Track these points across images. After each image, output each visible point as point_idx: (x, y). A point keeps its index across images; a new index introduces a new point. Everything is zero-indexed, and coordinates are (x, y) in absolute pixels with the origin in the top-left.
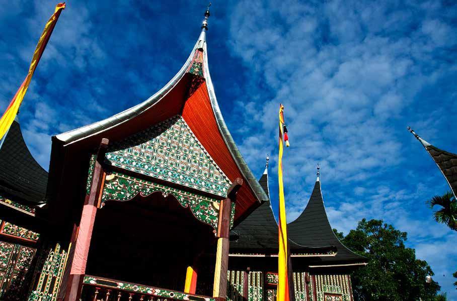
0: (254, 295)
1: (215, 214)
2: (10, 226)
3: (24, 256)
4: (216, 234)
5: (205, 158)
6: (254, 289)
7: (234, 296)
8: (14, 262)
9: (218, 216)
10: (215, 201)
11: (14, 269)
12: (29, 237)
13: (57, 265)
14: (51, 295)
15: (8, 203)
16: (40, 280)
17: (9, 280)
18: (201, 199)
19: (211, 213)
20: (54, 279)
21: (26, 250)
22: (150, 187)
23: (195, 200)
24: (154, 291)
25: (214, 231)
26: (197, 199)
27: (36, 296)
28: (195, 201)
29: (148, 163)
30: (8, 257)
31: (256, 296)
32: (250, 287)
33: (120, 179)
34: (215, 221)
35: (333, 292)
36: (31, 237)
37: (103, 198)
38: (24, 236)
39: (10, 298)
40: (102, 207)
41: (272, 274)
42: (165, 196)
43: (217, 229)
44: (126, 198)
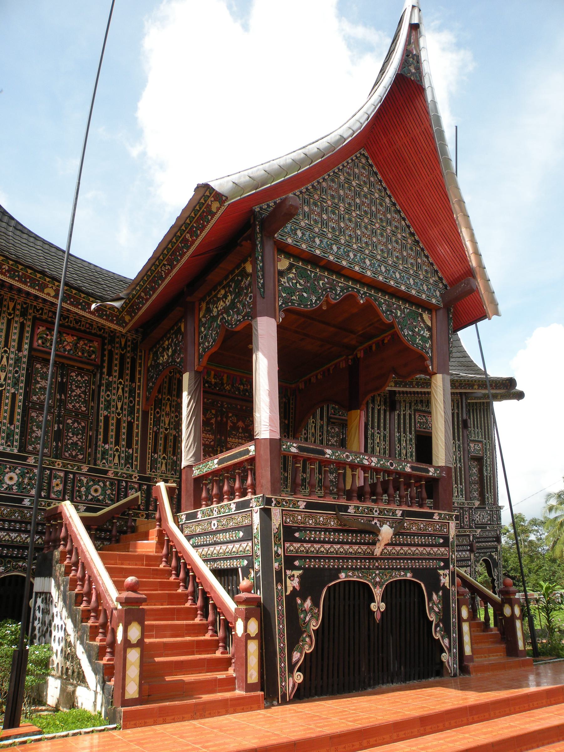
0: (402, 447)
1: (427, 334)
2: (47, 335)
3: (76, 386)
4: (430, 367)
5: (408, 235)
6: (402, 438)
7: (378, 449)
8: (63, 397)
9: (431, 337)
10: (425, 312)
11: (65, 409)
12: (80, 354)
13: (131, 402)
14: (130, 451)
15: (48, 294)
16: (111, 427)
17: (61, 426)
18: (407, 308)
19: (422, 332)
20: (130, 425)
21: (77, 376)
22: (340, 284)
23: (401, 311)
24: (369, 460)
25: (428, 362)
26: (402, 307)
27: (110, 452)
28: (400, 310)
29: (337, 242)
30: (85, 395)
31: (404, 448)
32: (397, 435)
33: (297, 268)
34: (428, 346)
35: (476, 439)
36: (83, 354)
37: (280, 304)
38: (72, 352)
39: (69, 455)
40: (281, 320)
41: (424, 416)
42: (362, 302)
43: (431, 358)
44: (311, 304)
